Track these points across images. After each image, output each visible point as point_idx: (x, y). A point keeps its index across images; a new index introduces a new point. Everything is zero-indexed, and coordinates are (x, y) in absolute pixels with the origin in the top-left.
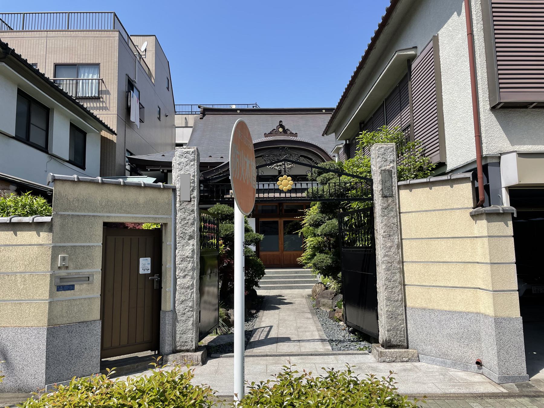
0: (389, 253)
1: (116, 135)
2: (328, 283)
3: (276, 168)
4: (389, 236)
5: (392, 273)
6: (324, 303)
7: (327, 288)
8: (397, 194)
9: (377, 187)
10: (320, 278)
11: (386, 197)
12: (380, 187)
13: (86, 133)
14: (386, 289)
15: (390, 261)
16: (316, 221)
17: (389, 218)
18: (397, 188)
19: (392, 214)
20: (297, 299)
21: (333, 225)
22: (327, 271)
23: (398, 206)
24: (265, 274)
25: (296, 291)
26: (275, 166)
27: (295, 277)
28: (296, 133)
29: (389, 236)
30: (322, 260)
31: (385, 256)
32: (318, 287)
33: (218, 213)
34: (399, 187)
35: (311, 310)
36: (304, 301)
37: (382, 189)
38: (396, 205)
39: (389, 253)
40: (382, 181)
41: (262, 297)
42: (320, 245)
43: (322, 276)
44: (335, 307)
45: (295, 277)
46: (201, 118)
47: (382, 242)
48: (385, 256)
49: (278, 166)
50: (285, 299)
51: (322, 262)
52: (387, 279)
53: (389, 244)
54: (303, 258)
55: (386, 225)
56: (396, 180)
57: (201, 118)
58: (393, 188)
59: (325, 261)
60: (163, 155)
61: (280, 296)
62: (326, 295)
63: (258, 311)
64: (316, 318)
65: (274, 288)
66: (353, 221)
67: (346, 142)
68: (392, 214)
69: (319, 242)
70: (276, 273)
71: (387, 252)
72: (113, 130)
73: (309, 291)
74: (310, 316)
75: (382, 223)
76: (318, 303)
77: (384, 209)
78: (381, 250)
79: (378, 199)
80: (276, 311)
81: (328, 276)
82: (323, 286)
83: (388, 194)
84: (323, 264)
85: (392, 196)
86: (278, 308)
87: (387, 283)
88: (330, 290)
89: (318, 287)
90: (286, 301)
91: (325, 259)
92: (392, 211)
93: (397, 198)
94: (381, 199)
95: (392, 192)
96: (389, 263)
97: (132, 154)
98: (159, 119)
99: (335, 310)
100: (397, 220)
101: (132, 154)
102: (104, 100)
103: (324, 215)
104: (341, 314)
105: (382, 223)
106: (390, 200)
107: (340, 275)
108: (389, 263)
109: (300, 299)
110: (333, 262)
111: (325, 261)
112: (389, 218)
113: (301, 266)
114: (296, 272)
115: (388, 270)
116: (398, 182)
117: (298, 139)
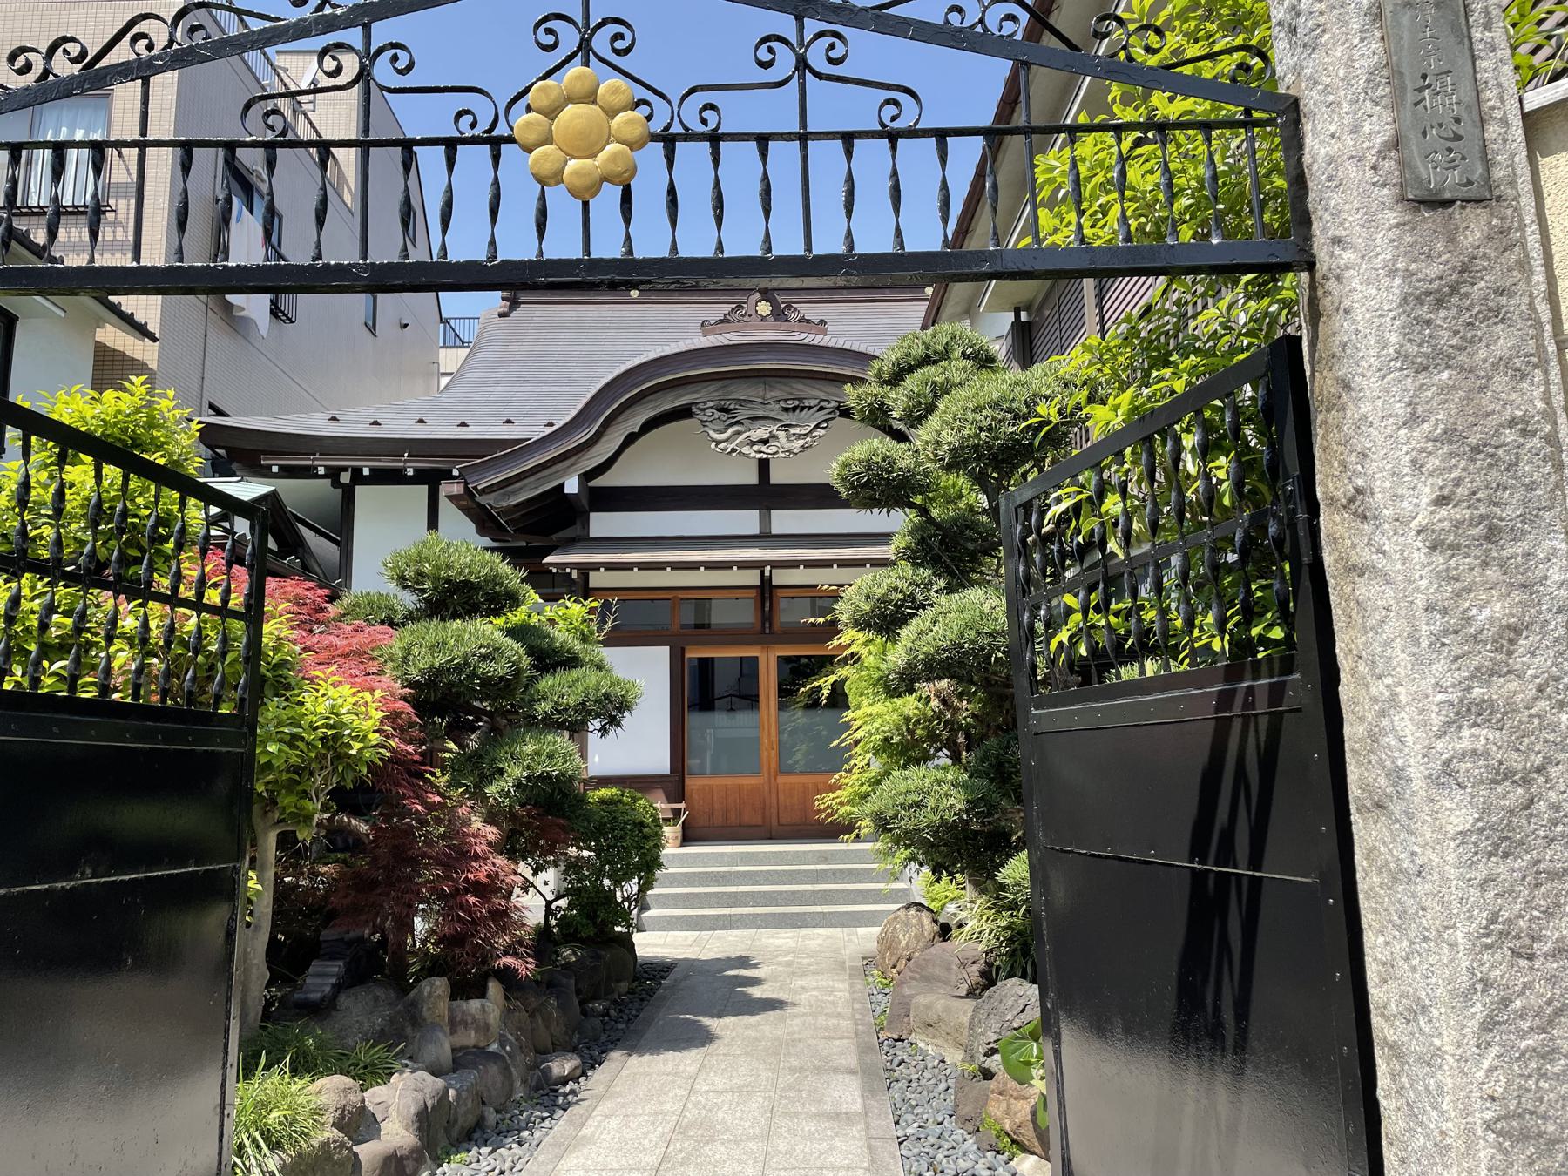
0: (1500, 690)
1: (154, 339)
2: (951, 908)
3: (746, 450)
4: (1493, 534)
5: (1539, 875)
6: (932, 1016)
7: (945, 931)
8: (1524, 186)
9: (1346, 140)
10: (919, 881)
11: (1437, 203)
12: (1378, 127)
13: (17, 318)
14: (1488, 1025)
15: (1515, 761)
16: (883, 600)
17: (1475, 382)
18: (1517, 133)
19: (1503, 346)
20: (810, 981)
21: (967, 615)
22: (964, 849)
23: (1539, 277)
24: (660, 866)
25: (817, 937)
26: (740, 444)
27: (819, 877)
28: (822, 321)
29: (1493, 534)
30: (915, 797)
31: (1468, 712)
32: (906, 923)
33: (420, 574)
34: (1532, 121)
35: (864, 1050)
36: (841, 988)
37: (1396, 144)
38: (1524, 265)
39: (1500, 690)
40: (1394, 75)
41: (660, 970)
42: (911, 732)
43: (926, 870)
44: (991, 1052)
45: (819, 877)
46: (502, 315)
47: (1426, 588)
48: (1468, 712)
49: (753, 443)
50: (755, 982)
51: (918, 805)
52: (1495, 932)
53: (1492, 610)
54: (843, 794)
55: (1451, 434)
56: (1508, 77)
57: (502, 315)
58: (1492, 131)
59: (931, 802)
60: (334, 419)
61: (743, 962)
62: (937, 971)
63: (591, 1063)
64: (883, 1106)
65: (729, 923)
66: (1113, 505)
67: (1017, 316)
68: (1504, 342)
69: (907, 719)
70: (825, 858)
71: (1478, 674)
72: (150, 328)
73: (866, 938)
74: (848, 1094)
75: (1414, 420)
76: (902, 1009)
77: (1429, 299)
78: (1419, 662)
79: (1370, 222)
80: (686, 1061)
81: (950, 874)
82: (926, 918)
83: (1455, 176)
84: (927, 817)
85: (1484, 196)
86: (703, 1038)
87: (1497, 965)
88: (959, 944)
89: (906, 923)
90: (756, 992)
91: (940, 787)
92: (1498, 315)
93: (1529, 216)
94: (1392, 217)
95: (1488, 163)
96: (1502, 775)
97: (220, 413)
98: (372, 328)
99: (988, 1075)
100: (1547, 397)
101: (220, 413)
102: (121, 217)
103: (925, 573)
104: (1023, 1109)
105: (1414, 420)
106: (1474, 227)
107: (1016, 870)
108: (1502, 775)
109: (823, 981)
110: (972, 804)
111: (931, 802)
112: (1475, 382)
113: (834, 830)
114: (825, 858)
115: (1503, 844)
116: (1523, 85)
117: (827, 340)
